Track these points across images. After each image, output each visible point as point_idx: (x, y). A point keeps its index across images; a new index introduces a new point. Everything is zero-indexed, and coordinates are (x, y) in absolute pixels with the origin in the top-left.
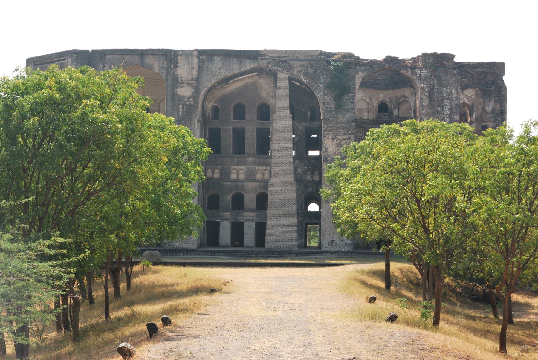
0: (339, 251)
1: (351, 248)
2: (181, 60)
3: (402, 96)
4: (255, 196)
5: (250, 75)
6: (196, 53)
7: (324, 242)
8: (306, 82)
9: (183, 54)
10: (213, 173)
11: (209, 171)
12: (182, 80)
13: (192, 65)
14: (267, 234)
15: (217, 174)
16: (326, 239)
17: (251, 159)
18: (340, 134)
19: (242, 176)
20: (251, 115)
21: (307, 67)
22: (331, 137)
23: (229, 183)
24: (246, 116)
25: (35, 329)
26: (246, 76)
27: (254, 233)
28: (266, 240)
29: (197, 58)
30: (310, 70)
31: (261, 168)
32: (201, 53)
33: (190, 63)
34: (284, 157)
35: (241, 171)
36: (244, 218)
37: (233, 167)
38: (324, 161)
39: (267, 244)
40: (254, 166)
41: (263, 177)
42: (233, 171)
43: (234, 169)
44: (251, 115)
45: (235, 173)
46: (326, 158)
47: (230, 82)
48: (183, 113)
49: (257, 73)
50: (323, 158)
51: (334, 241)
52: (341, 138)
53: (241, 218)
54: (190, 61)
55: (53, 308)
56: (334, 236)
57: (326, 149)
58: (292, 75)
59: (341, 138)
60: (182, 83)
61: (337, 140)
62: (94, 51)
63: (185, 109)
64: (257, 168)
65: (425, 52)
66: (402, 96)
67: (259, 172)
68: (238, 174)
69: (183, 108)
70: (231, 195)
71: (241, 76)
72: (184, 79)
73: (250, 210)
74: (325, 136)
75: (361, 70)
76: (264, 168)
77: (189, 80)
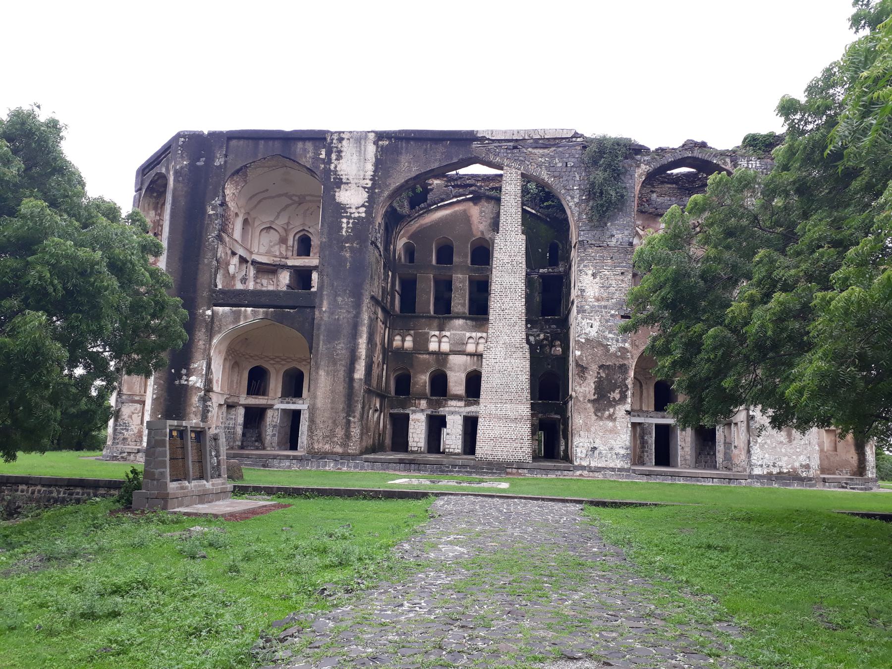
0: (606, 468)
1: (627, 463)
2: (347, 147)
3: (697, 224)
4: (463, 376)
5: (461, 198)
6: (372, 136)
7: (579, 450)
8: (550, 182)
9: (352, 137)
10: (403, 341)
11: (398, 338)
12: (348, 179)
13: (365, 154)
14: (478, 431)
15: (409, 343)
16: (581, 444)
17: (460, 322)
18: (606, 266)
19: (445, 347)
20: (462, 257)
21: (553, 157)
22: (590, 272)
23: (426, 356)
24: (454, 258)
25: (622, 436)
26: (455, 200)
27: (461, 433)
28: (478, 443)
29: (374, 144)
30: (557, 161)
31: (474, 334)
32: (380, 136)
33: (362, 152)
34: (511, 305)
35: (445, 339)
36: (447, 409)
37: (433, 333)
38: (578, 313)
39: (478, 450)
40: (465, 332)
41: (476, 348)
42: (434, 339)
43: (434, 335)
44: (462, 257)
45: (435, 342)
46: (582, 306)
47: (432, 207)
48: (347, 231)
49: (471, 196)
50: (577, 306)
51: (595, 448)
52: (608, 273)
53: (441, 409)
54: (363, 148)
55: (717, 428)
56: (597, 441)
57: (583, 291)
58: (527, 171)
59: (608, 273)
60: (347, 183)
61: (601, 278)
62: (212, 134)
63: (350, 225)
64: (468, 334)
65: (753, 133)
66: (697, 224)
67: (471, 341)
68: (440, 342)
69: (348, 223)
70: (428, 374)
71: (443, 200)
72: (351, 178)
73: (457, 398)
74: (580, 271)
75: (644, 161)
76: (479, 335)
77: (359, 179)
